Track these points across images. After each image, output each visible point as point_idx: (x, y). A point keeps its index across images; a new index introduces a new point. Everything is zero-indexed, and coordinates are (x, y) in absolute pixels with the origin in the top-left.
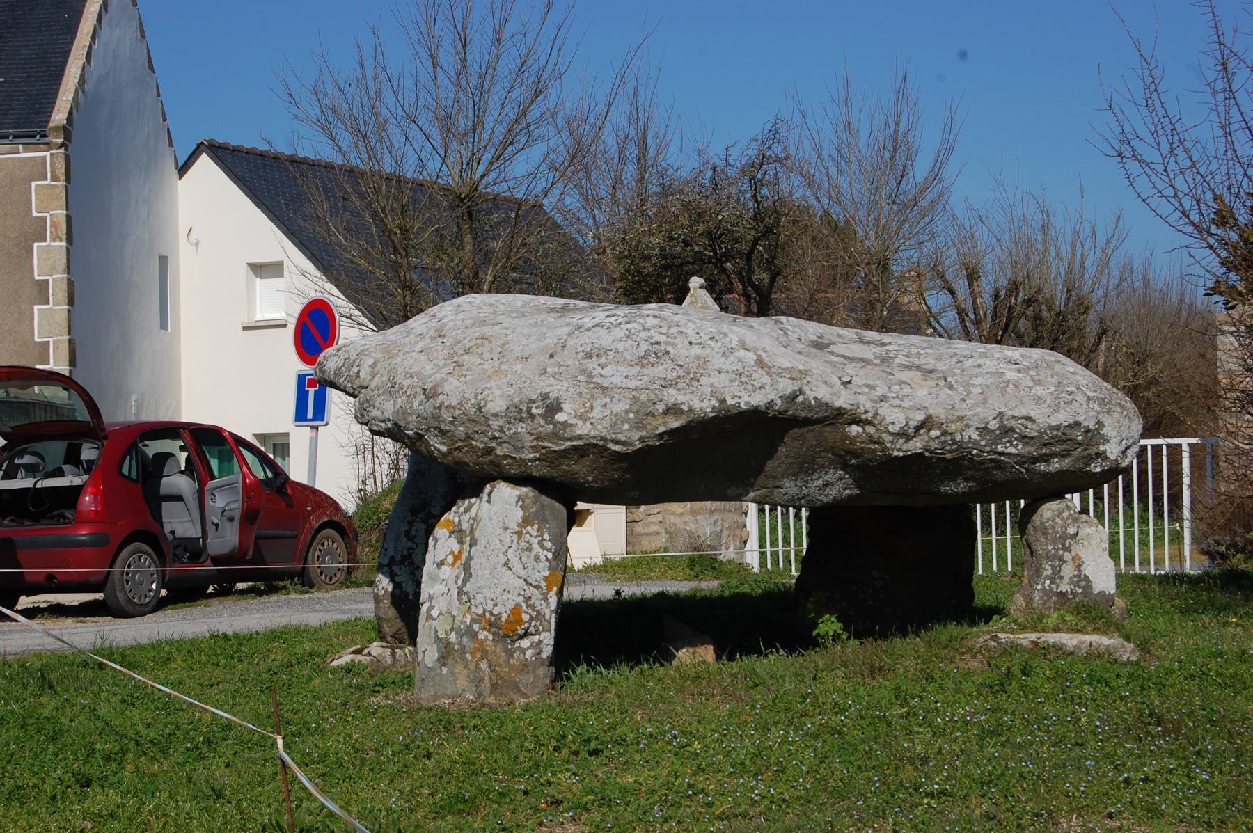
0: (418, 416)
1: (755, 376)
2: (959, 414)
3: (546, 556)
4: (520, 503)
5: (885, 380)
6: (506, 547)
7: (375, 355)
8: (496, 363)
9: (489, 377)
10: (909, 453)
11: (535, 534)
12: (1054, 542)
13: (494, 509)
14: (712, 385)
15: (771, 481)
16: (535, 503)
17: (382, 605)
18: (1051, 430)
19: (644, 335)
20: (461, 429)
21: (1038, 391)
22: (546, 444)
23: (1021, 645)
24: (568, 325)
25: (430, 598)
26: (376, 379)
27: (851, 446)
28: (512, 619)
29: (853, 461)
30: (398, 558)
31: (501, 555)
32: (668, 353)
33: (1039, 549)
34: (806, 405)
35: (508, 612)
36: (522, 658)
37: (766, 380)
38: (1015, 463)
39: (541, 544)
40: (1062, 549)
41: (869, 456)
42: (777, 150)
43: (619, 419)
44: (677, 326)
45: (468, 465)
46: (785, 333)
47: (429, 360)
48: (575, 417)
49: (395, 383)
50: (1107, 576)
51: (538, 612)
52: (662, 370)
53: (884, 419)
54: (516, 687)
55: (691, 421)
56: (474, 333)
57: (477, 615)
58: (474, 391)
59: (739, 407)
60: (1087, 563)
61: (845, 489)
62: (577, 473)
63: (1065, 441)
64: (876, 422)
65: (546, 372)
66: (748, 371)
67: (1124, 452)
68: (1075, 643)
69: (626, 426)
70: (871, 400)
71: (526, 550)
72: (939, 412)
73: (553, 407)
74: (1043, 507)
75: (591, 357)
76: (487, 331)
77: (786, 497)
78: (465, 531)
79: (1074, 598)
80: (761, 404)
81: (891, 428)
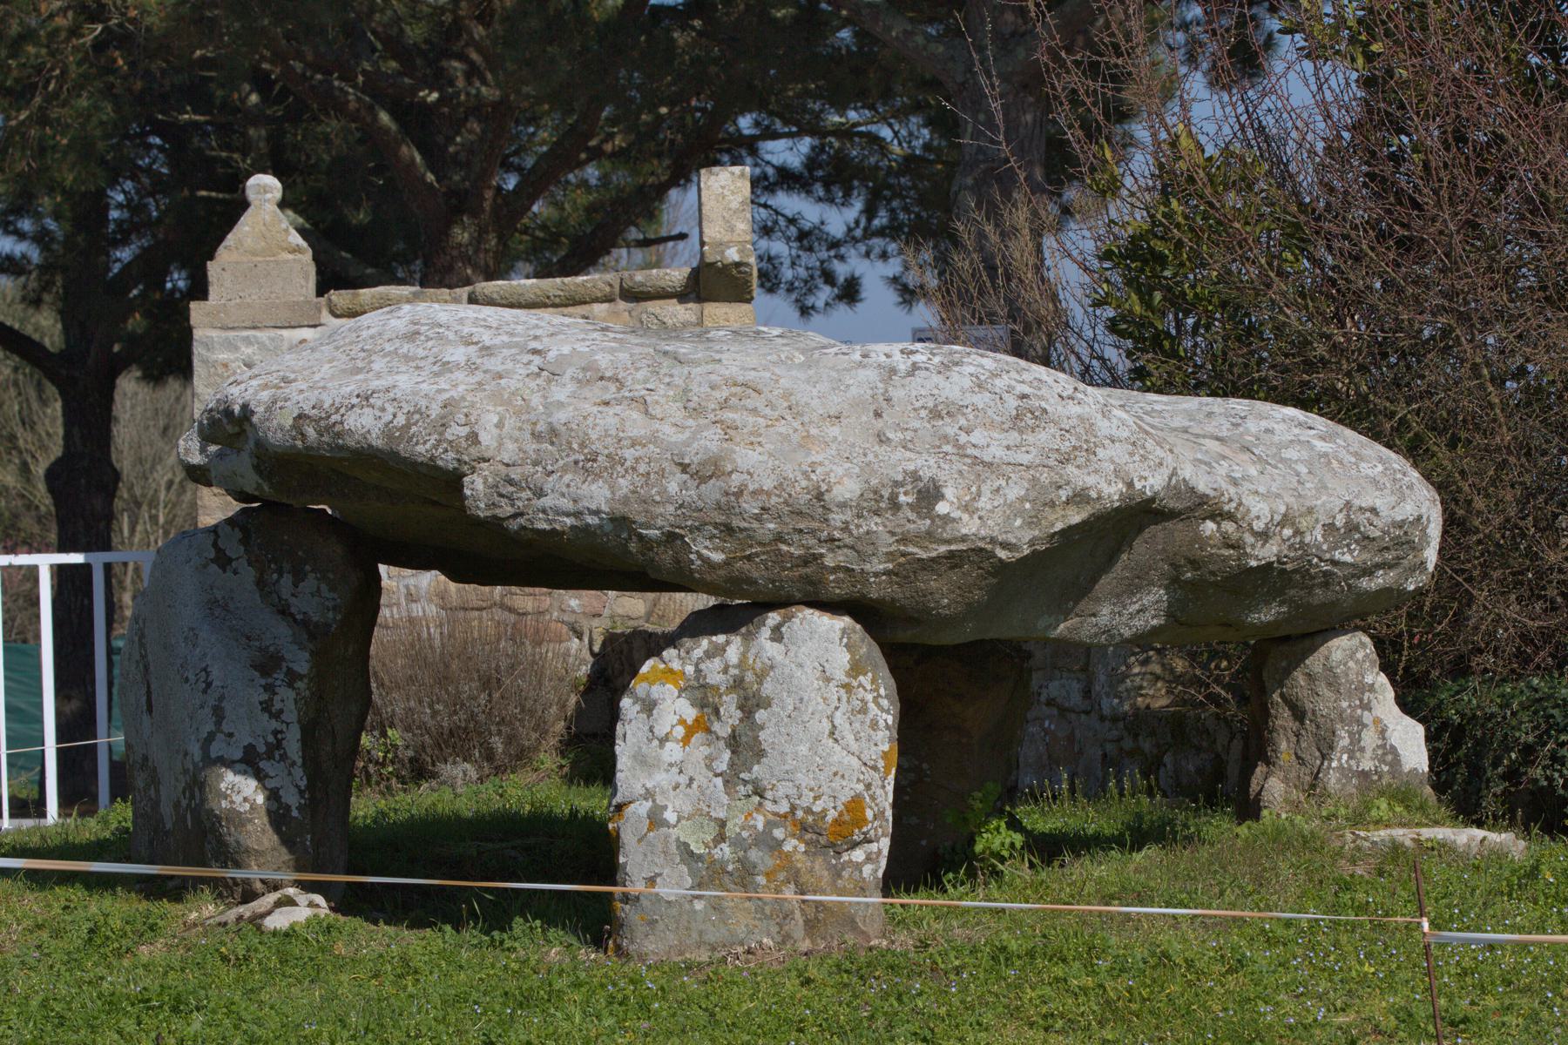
4: (845, 640)
6: (833, 706)
17: (249, 827)
20: (771, 526)
22: (911, 549)
28: (847, 818)
30: (262, 749)
31: (825, 720)
43: (1014, 509)
45: (756, 582)
52: (1045, 437)
53: (1248, 511)
59: (1144, 493)
60: (1391, 727)
71: (859, 712)
73: (929, 495)
74: (1330, 643)
79: (1380, 778)
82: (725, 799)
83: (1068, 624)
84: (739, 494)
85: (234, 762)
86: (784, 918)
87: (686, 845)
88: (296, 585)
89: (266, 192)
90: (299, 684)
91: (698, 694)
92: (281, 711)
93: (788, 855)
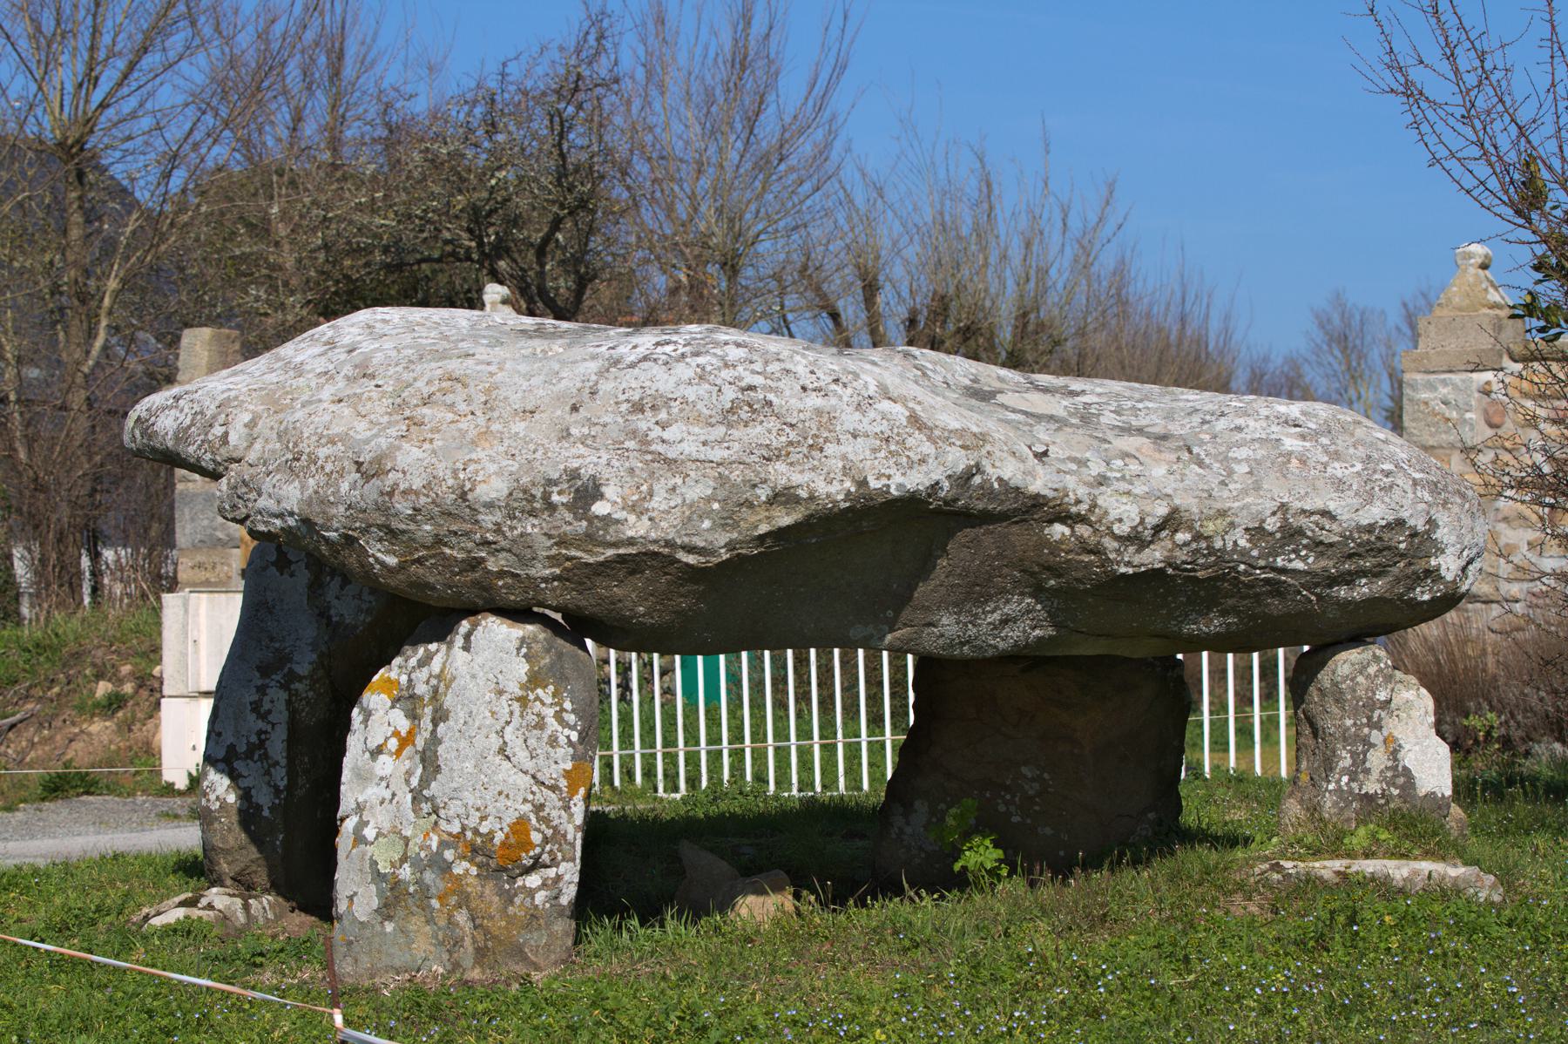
0: (350, 507)
1: (910, 442)
2: (1218, 505)
3: (568, 737)
4: (524, 650)
5: (1098, 452)
7: (251, 407)
8: (481, 420)
9: (473, 442)
10: (1143, 569)
11: (549, 700)
12: (1355, 713)
13: (479, 660)
14: (844, 457)
15: (919, 615)
16: (548, 651)
17: (216, 825)
18: (1359, 532)
19: (726, 374)
20: (428, 528)
21: (1337, 469)
22: (573, 553)
23: (1321, 878)
24: (594, 357)
25: (360, 808)
26: (258, 446)
27: (1051, 558)
28: (512, 841)
29: (1052, 582)
30: (242, 748)
32: (769, 404)
33: (1329, 725)
34: (987, 491)
35: (507, 829)
36: (528, 905)
37: (928, 448)
38: (1303, 586)
39: (558, 717)
40: (1368, 725)
41: (1079, 575)
42: (603, 68)
43: (695, 511)
44: (779, 360)
45: (433, 588)
46: (924, 374)
47: (359, 414)
48: (623, 509)
49: (301, 453)
50: (1440, 768)
51: (555, 828)
52: (761, 432)
53: (1106, 513)
54: (518, 952)
55: (811, 516)
56: (432, 369)
57: (450, 834)
58: (450, 465)
59: (888, 492)
60: (1407, 747)
61: (1034, 628)
62: (620, 601)
63: (1380, 551)
64: (1093, 519)
65: (569, 434)
66: (898, 434)
67: (1464, 569)
68: (1405, 874)
69: (707, 524)
70: (1085, 484)
71: (535, 727)
72: (1188, 503)
73: (587, 493)
74: (1337, 657)
75: (642, 411)
76: (453, 365)
77: (941, 642)
78: (421, 698)
79: (1387, 802)
80: (921, 488)
81: (1116, 529)
82: (411, 816)
83: (898, 634)
84: (391, 494)
85: (217, 761)
86: (454, 945)
87: (376, 863)
88: (342, 588)
89: (1470, 258)
90: (297, 686)
91: (409, 705)
92: (269, 712)
93: (459, 878)
